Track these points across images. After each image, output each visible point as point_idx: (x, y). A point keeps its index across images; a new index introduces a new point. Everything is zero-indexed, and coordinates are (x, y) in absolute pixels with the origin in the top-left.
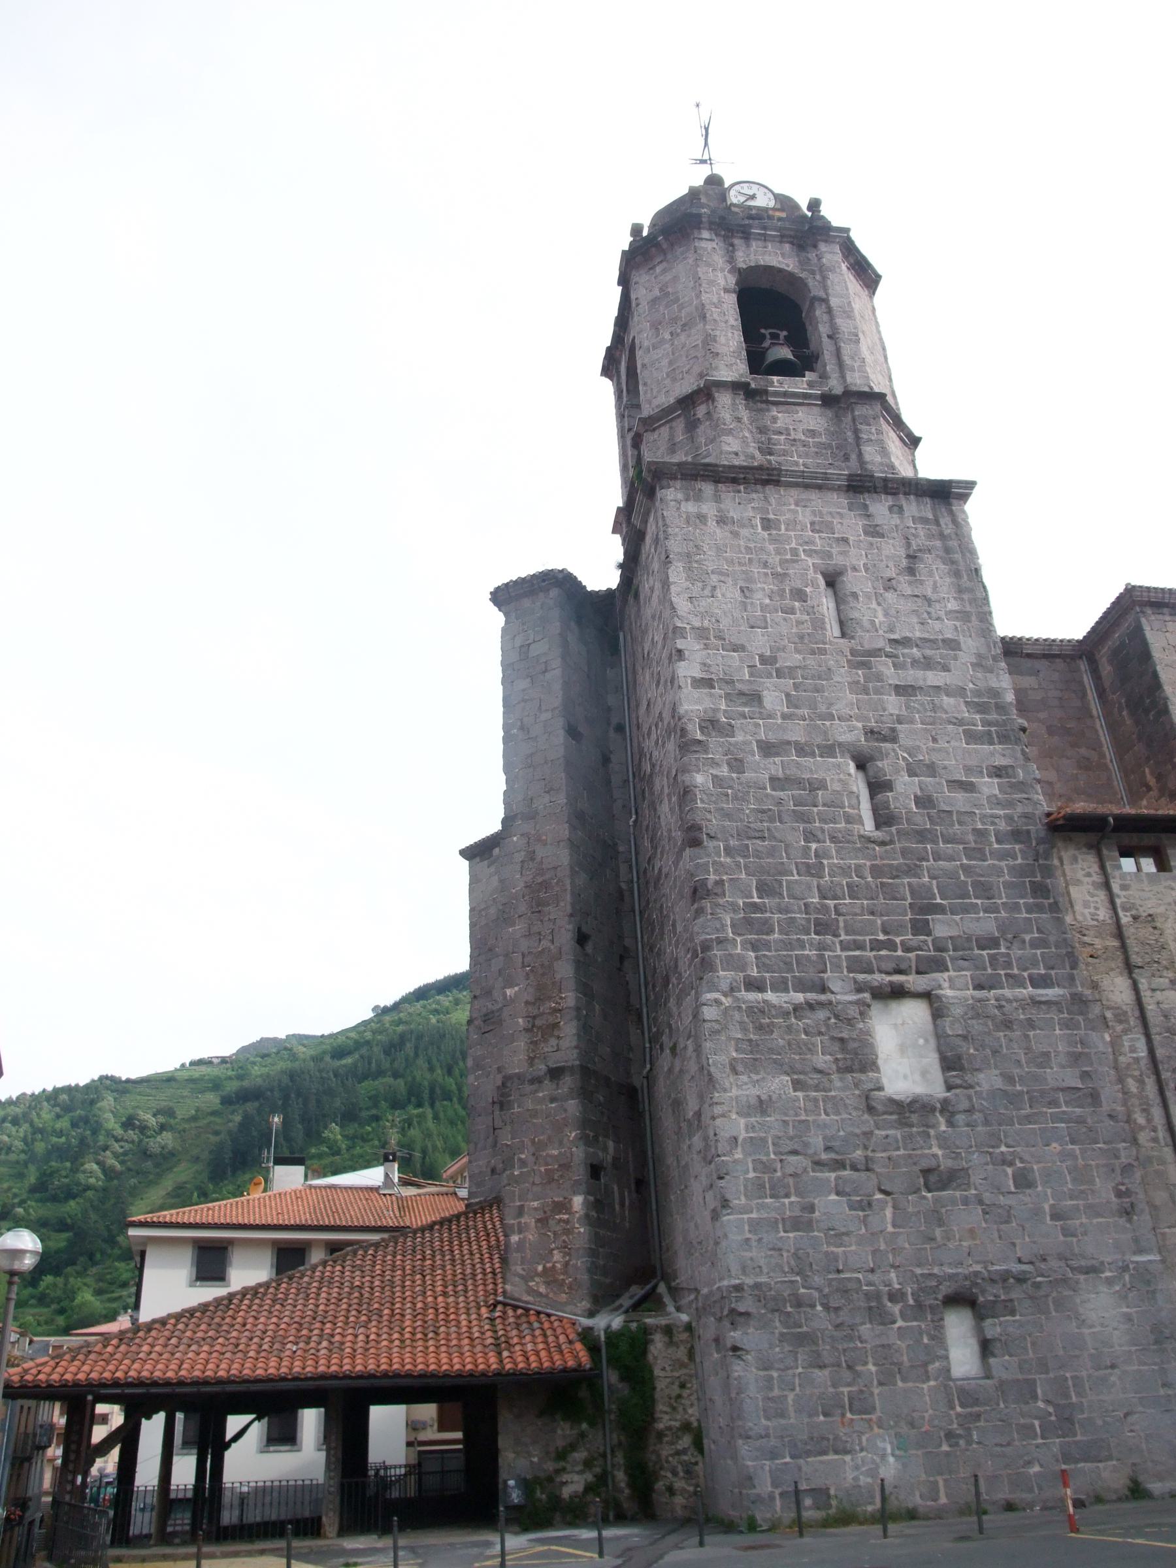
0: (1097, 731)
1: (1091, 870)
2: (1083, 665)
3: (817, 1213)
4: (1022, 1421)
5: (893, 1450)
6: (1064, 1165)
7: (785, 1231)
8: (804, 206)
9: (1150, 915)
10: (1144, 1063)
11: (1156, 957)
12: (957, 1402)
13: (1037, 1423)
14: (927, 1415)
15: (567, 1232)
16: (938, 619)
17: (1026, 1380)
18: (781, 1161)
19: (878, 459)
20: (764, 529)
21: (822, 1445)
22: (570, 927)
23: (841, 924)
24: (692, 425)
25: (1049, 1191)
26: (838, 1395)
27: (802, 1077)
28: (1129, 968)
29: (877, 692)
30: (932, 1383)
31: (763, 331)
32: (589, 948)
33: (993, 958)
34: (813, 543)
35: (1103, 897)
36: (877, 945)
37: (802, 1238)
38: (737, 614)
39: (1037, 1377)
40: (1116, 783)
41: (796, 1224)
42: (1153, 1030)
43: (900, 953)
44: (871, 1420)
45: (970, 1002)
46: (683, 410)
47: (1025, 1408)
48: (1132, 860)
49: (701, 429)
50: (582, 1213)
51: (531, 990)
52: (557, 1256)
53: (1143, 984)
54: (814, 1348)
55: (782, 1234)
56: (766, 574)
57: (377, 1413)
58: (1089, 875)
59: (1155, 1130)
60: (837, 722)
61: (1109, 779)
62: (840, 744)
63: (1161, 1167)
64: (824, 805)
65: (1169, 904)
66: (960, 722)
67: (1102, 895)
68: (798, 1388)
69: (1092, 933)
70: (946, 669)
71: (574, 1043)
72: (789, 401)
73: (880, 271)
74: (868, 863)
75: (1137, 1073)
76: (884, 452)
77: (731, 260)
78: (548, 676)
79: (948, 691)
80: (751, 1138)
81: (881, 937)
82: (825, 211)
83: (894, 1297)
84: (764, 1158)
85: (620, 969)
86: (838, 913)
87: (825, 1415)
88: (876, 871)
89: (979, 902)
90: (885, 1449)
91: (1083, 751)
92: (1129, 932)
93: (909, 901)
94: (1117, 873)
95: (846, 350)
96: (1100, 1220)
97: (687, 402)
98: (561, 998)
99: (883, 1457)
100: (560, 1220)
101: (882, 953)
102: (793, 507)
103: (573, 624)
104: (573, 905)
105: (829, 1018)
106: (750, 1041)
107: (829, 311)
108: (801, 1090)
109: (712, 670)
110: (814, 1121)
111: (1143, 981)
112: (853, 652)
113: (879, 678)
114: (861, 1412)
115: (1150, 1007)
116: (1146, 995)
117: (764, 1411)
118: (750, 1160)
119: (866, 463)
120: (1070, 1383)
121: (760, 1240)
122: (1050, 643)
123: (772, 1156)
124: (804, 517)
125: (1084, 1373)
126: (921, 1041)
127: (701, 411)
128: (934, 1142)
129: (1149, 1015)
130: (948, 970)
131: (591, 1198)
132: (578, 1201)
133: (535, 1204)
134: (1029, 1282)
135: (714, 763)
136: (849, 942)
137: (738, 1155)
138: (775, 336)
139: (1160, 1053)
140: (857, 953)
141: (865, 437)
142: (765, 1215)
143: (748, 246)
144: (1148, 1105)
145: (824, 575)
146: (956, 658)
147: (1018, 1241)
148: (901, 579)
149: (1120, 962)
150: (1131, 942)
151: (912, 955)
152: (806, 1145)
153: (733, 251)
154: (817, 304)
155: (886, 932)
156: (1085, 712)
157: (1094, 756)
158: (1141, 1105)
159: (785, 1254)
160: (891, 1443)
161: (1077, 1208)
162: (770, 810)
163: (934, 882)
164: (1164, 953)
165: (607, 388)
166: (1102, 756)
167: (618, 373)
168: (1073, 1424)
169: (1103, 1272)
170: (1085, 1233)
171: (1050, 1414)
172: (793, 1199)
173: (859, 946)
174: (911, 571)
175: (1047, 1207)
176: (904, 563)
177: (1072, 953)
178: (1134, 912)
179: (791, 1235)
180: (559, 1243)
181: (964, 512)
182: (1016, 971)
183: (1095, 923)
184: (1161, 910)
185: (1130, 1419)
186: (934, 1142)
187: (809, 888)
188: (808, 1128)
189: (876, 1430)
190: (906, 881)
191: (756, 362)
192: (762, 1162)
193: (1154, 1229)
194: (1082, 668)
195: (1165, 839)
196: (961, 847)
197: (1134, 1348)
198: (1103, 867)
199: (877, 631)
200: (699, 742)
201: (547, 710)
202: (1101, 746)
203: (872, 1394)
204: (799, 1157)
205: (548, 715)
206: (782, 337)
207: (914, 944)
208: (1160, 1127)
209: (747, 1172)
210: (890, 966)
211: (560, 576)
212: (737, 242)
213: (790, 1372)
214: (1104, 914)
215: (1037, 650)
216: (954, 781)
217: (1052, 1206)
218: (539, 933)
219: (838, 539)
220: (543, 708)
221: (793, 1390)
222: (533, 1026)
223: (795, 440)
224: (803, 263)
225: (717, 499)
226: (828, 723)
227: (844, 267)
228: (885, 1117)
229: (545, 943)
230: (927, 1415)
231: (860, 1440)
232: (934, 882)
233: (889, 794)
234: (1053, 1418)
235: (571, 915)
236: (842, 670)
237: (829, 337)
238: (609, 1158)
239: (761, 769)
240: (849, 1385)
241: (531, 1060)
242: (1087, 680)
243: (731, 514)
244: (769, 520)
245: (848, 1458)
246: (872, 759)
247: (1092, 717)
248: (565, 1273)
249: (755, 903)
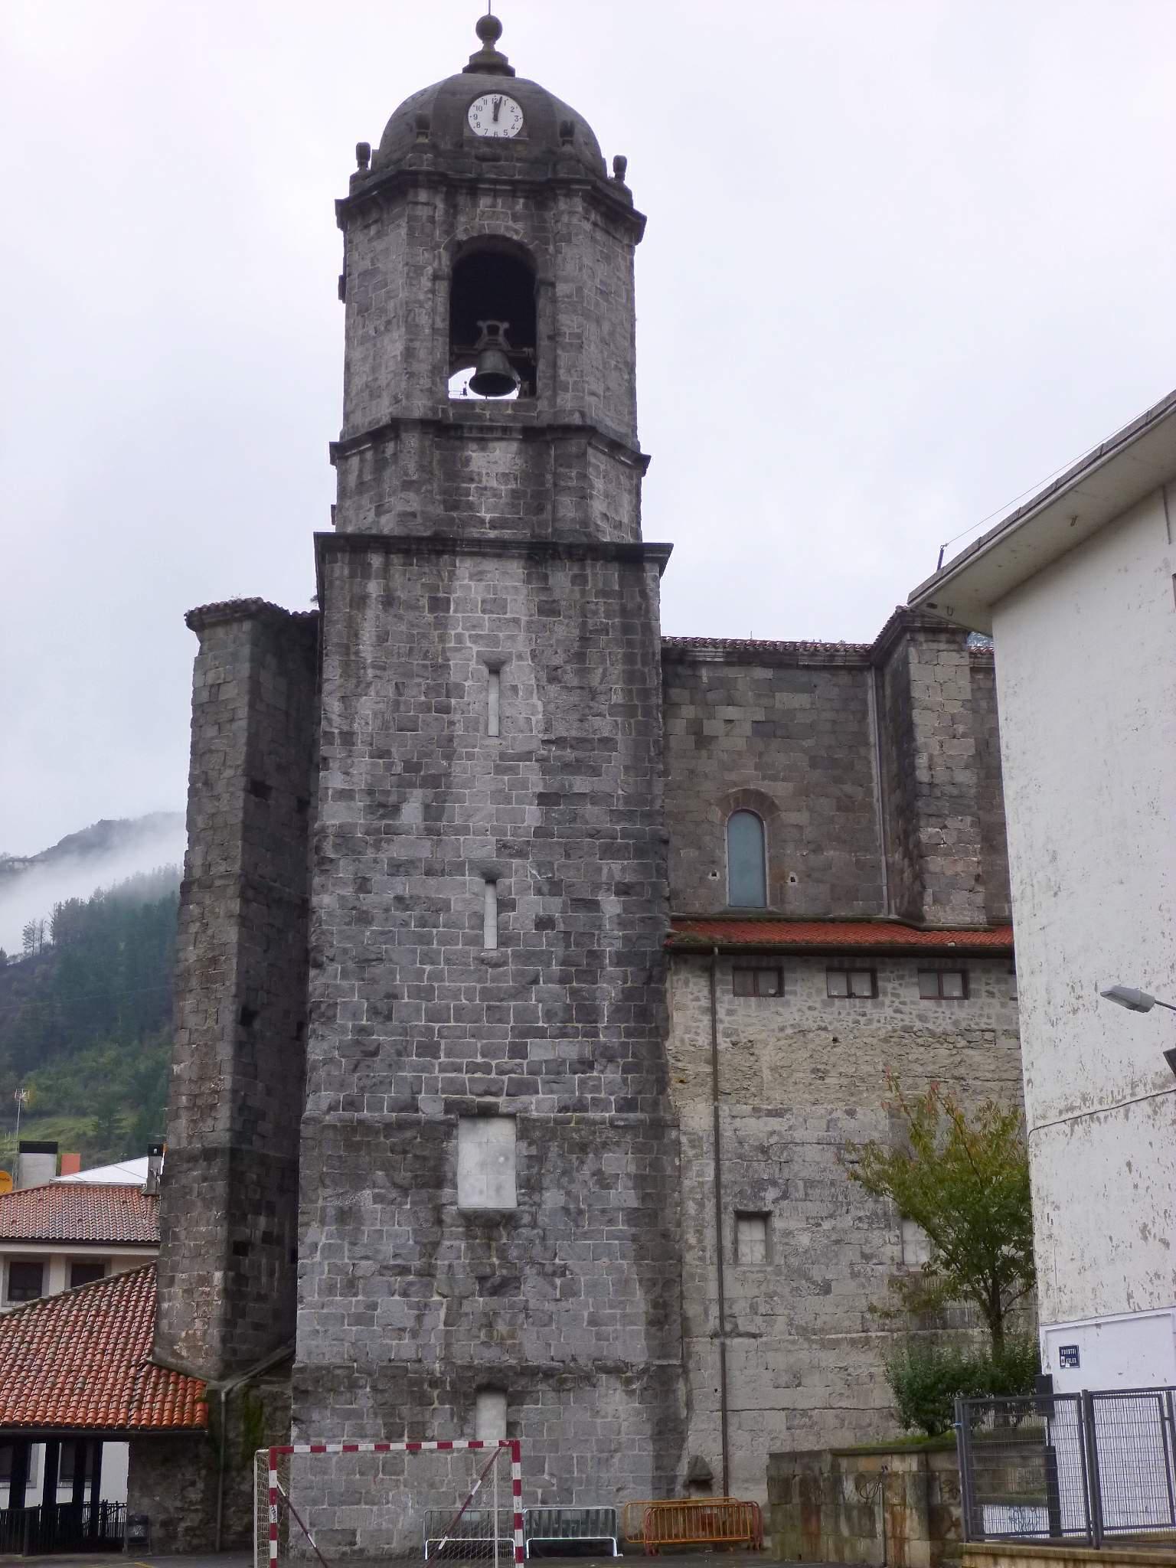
6: (610, 1278)
9: (750, 1041)
10: (708, 1188)
11: (745, 1084)
13: (540, 1491)
15: (208, 1303)
18: (354, 1264)
21: (353, 1496)
22: (233, 1008)
25: (591, 1301)
28: (716, 1093)
32: (257, 1025)
33: (582, 1082)
36: (473, 1068)
41: (359, 1320)
43: (493, 1075)
44: (398, 1480)
45: (552, 1124)
47: (532, 1479)
50: (220, 1287)
51: (195, 1068)
52: (198, 1324)
53: (725, 1110)
54: (359, 1422)
55: (346, 1327)
56: (425, 666)
57: (107, 1446)
64: (444, 927)
65: (773, 1030)
67: (706, 1020)
69: (687, 1058)
70: (595, 772)
71: (228, 1126)
74: (479, 986)
75: (698, 1196)
79: (593, 798)
80: (330, 1244)
81: (479, 1060)
83: (434, 1383)
84: (339, 1262)
86: (440, 1036)
87: (362, 1474)
88: (486, 994)
89: (580, 1025)
91: (848, 788)
92: (723, 1059)
98: (220, 1080)
100: (203, 1292)
101: (476, 1075)
104: (238, 985)
105: (416, 1138)
106: (340, 1157)
109: (355, 780)
114: (391, 1474)
115: (727, 1133)
123: (347, 1261)
127: (390, 448)
128: (494, 1253)
131: (231, 1274)
132: (218, 1276)
133: (184, 1276)
135: (343, 883)
136: (448, 1064)
137: (318, 1257)
139: (725, 1178)
145: (487, 664)
147: (553, 1343)
148: (568, 668)
149: (708, 1089)
151: (505, 1078)
152: (377, 1251)
153: (455, 215)
156: (862, 738)
157: (859, 793)
159: (346, 1344)
161: (613, 1317)
162: (391, 931)
163: (540, 1005)
164: (756, 1080)
172: (360, 1298)
173: (458, 1069)
175: (586, 1314)
178: (734, 1038)
179: (354, 1328)
180: (200, 1312)
183: (693, 1049)
185: (621, 1493)
186: (494, 1253)
188: (381, 1237)
190: (512, 1003)
193: (682, 1337)
196: (573, 969)
198: (712, 992)
201: (230, 767)
204: (371, 1262)
207: (507, 1067)
209: (322, 1273)
210: (481, 1088)
211: (254, 608)
217: (591, 1314)
218: (206, 1011)
219: (508, 620)
220: (229, 763)
222: (194, 1104)
223: (485, 488)
224: (540, 230)
228: (453, 1229)
229: (210, 1023)
231: (388, 1495)
234: (555, 1488)
235: (235, 996)
241: (190, 1137)
243: (398, 593)
245: (375, 1508)
246: (500, 875)
248: (204, 1340)
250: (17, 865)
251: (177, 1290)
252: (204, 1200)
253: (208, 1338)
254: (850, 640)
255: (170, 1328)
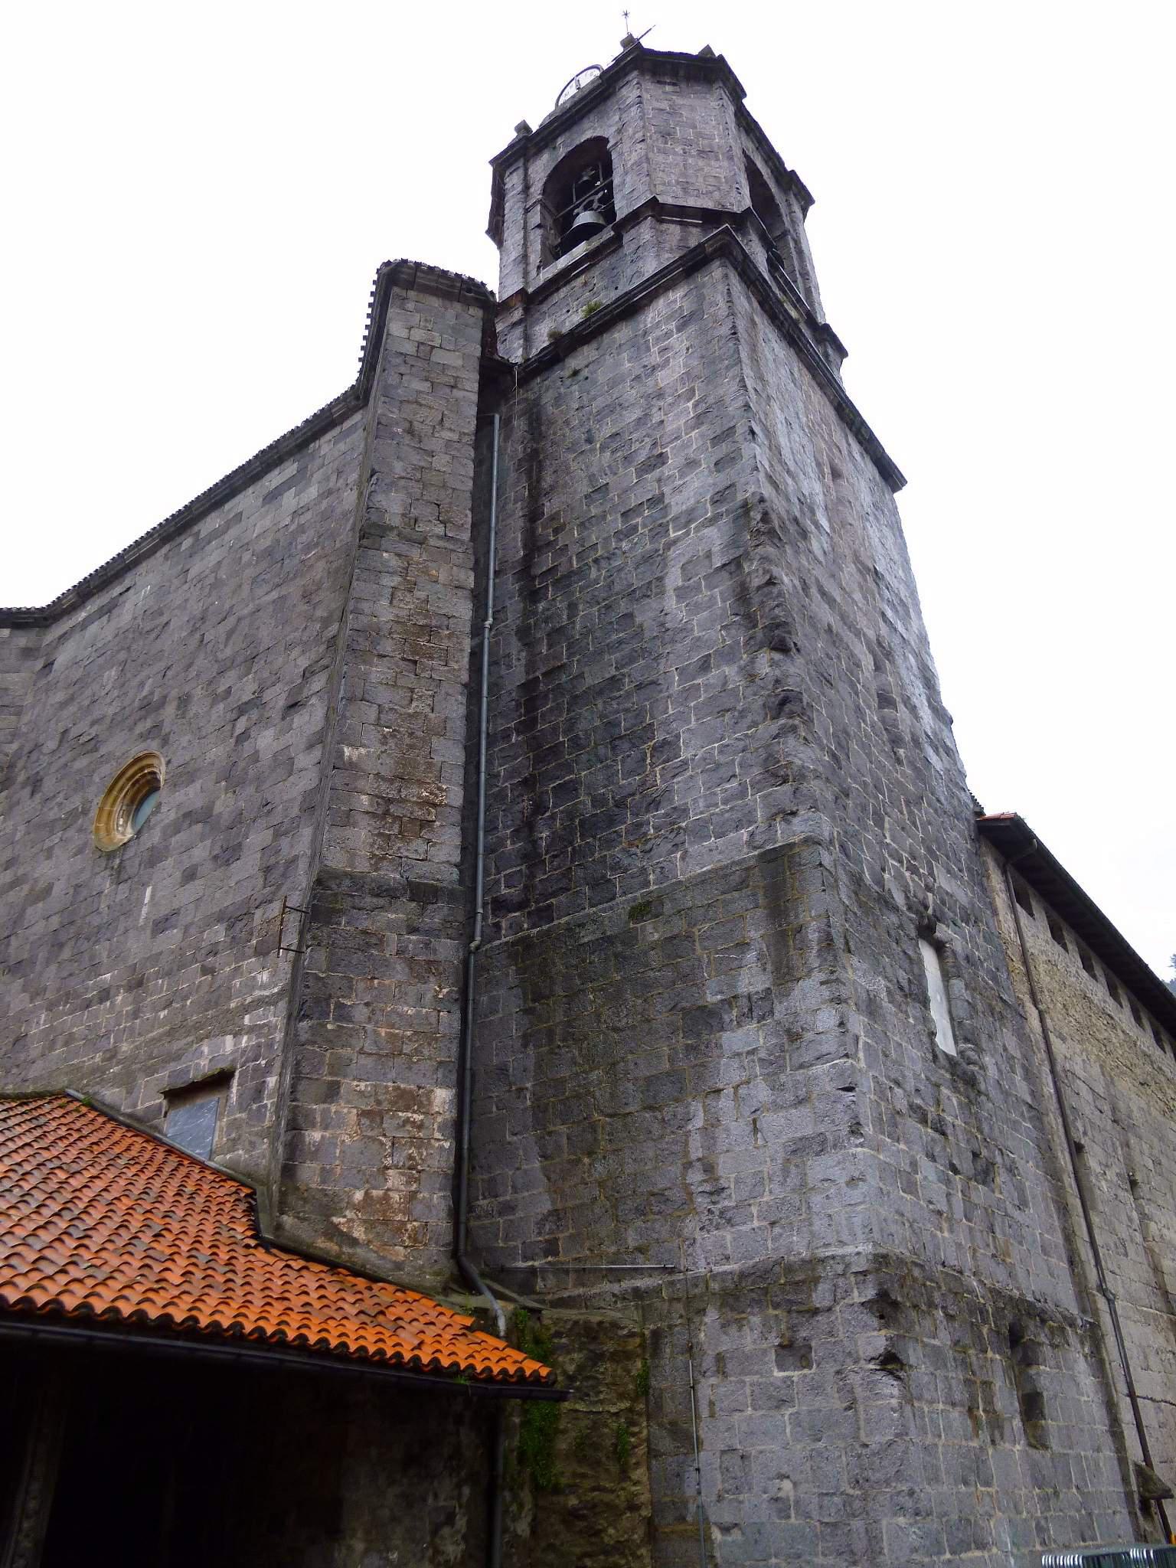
52: (394, 1179)
98: (440, 789)
180: (400, 1158)
218: (412, 690)
248: (407, 1212)
250: (732, 455)
251: (346, 1110)
252: (411, 962)
253: (418, 1209)
254: (965, 738)
255: (323, 1182)
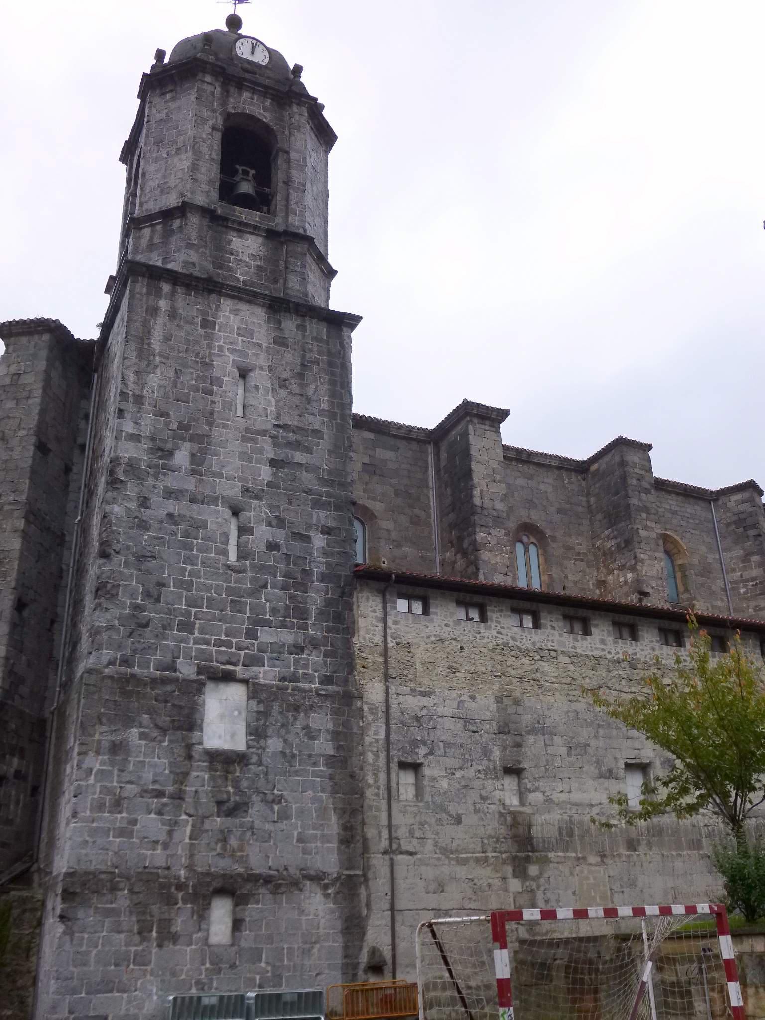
0: (429, 498)
1: (377, 608)
2: (430, 449)
3: (138, 826)
4: (248, 975)
5: (157, 991)
7: (113, 837)
8: (292, 67)
9: (408, 643)
12: (208, 961)
13: (258, 977)
14: (185, 969)
16: (312, 414)
17: (257, 948)
18: (121, 788)
19: (297, 287)
20: (202, 327)
22: (12, 597)
23: (197, 626)
24: (168, 233)
25: (299, 823)
26: (128, 952)
27: (147, 730)
28: (387, 677)
29: (258, 461)
30: (193, 947)
31: (237, 167)
32: (26, 613)
33: (296, 661)
34: (236, 344)
35: (380, 627)
36: (219, 643)
37: (124, 842)
38: (169, 390)
39: (264, 946)
40: (434, 537)
41: (122, 833)
42: (393, 722)
46: (164, 219)
48: (406, 601)
49: (174, 239)
53: (393, 690)
54: (117, 919)
56: (196, 362)
58: (374, 611)
59: (378, 788)
60: (224, 480)
61: (430, 533)
62: (223, 497)
63: (377, 814)
65: (423, 637)
66: (308, 492)
67: (380, 626)
68: (100, 947)
70: (309, 451)
72: (242, 228)
73: (337, 133)
74: (225, 585)
75: (375, 749)
76: (304, 280)
77: (224, 104)
78: (30, 402)
79: (307, 468)
80: (102, 770)
81: (223, 638)
82: (304, 78)
83: (180, 887)
85: (50, 630)
87: (116, 965)
88: (230, 591)
89: (296, 621)
90: (152, 990)
91: (417, 511)
92: (392, 653)
93: (248, 614)
94: (393, 612)
95: (294, 196)
96: (328, 845)
97: (167, 215)
99: (150, 995)
101: (221, 649)
102: (227, 314)
103: (57, 363)
104: (17, 580)
107: (288, 162)
108: (145, 739)
110: (149, 762)
111: (393, 687)
112: (247, 430)
113: (261, 451)
115: (394, 706)
116: (393, 697)
117: (73, 961)
118: (98, 785)
119: (288, 288)
120: (285, 951)
121: (94, 842)
122: (410, 429)
123: (115, 784)
124: (234, 322)
125: (296, 946)
126: (236, 713)
127: (177, 223)
128: (229, 783)
129: (392, 711)
130: (264, 666)
134: (273, 883)
136: (200, 639)
138: (245, 173)
139: (393, 737)
140: (204, 647)
141: (292, 268)
142: (102, 825)
143: (240, 95)
144: (378, 771)
145: (239, 369)
146: (318, 445)
149: (381, 673)
150: (392, 662)
151: (242, 653)
152: (140, 778)
153: (227, 96)
154: (281, 153)
155: (227, 635)
156: (424, 483)
157: (423, 515)
158: (373, 770)
160: (157, 987)
161: (315, 836)
164: (412, 671)
165: (122, 170)
166: (429, 516)
167: (132, 164)
168: (282, 979)
169: (323, 880)
170: (317, 853)
171: (268, 972)
172: (124, 815)
173: (207, 643)
174: (301, 375)
176: (298, 369)
177: (351, 663)
178: (398, 640)
179: (117, 840)
181: (349, 337)
182: (310, 672)
183: (371, 645)
184: (416, 641)
185: (319, 977)
186: (229, 783)
187: (180, 597)
189: (149, 977)
190: (248, 600)
191: (227, 192)
192: (106, 787)
194: (429, 450)
195: (430, 592)
196: (292, 581)
197: (332, 931)
198: (385, 608)
199: (267, 417)
200: (122, 481)
201: (24, 429)
202: (430, 508)
203: (151, 953)
204: (133, 786)
205: (24, 432)
206: (250, 175)
207: (244, 645)
208: (382, 786)
210: (224, 658)
212: (232, 89)
213: (97, 935)
214: (378, 639)
215: (401, 433)
216: (298, 534)
217: (299, 833)
219: (255, 344)
220: (23, 426)
221: (96, 947)
223: (240, 261)
225: (172, 296)
226: (218, 480)
227: (308, 127)
228: (200, 763)
230: (185, 969)
232: (268, 604)
233: (250, 537)
234: (269, 974)
235: (14, 588)
236: (237, 442)
237: (284, 182)
238: (12, 771)
239: (162, 508)
240: (136, 945)
242: (431, 460)
243: (181, 311)
244: (208, 321)
245: (125, 995)
246: (243, 510)
247: (428, 486)
249: (139, 604)
